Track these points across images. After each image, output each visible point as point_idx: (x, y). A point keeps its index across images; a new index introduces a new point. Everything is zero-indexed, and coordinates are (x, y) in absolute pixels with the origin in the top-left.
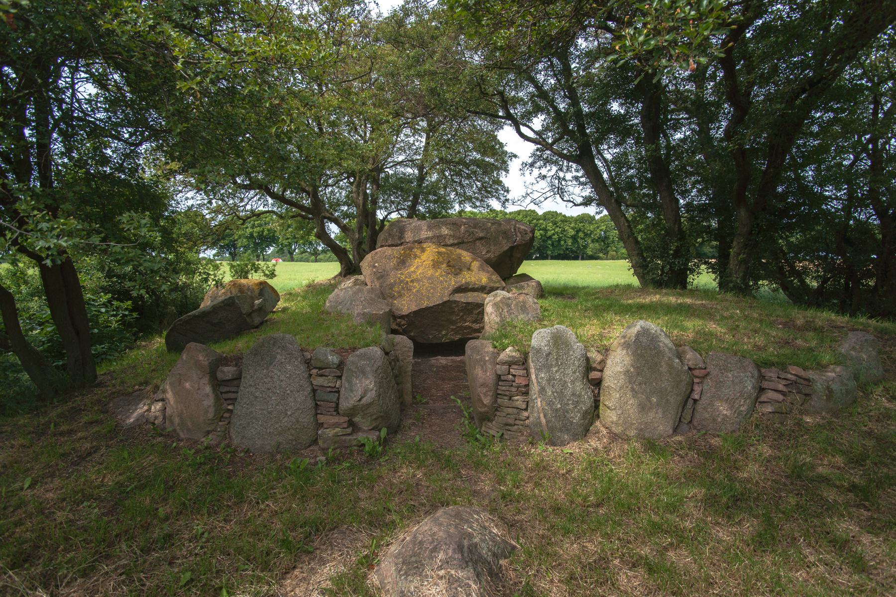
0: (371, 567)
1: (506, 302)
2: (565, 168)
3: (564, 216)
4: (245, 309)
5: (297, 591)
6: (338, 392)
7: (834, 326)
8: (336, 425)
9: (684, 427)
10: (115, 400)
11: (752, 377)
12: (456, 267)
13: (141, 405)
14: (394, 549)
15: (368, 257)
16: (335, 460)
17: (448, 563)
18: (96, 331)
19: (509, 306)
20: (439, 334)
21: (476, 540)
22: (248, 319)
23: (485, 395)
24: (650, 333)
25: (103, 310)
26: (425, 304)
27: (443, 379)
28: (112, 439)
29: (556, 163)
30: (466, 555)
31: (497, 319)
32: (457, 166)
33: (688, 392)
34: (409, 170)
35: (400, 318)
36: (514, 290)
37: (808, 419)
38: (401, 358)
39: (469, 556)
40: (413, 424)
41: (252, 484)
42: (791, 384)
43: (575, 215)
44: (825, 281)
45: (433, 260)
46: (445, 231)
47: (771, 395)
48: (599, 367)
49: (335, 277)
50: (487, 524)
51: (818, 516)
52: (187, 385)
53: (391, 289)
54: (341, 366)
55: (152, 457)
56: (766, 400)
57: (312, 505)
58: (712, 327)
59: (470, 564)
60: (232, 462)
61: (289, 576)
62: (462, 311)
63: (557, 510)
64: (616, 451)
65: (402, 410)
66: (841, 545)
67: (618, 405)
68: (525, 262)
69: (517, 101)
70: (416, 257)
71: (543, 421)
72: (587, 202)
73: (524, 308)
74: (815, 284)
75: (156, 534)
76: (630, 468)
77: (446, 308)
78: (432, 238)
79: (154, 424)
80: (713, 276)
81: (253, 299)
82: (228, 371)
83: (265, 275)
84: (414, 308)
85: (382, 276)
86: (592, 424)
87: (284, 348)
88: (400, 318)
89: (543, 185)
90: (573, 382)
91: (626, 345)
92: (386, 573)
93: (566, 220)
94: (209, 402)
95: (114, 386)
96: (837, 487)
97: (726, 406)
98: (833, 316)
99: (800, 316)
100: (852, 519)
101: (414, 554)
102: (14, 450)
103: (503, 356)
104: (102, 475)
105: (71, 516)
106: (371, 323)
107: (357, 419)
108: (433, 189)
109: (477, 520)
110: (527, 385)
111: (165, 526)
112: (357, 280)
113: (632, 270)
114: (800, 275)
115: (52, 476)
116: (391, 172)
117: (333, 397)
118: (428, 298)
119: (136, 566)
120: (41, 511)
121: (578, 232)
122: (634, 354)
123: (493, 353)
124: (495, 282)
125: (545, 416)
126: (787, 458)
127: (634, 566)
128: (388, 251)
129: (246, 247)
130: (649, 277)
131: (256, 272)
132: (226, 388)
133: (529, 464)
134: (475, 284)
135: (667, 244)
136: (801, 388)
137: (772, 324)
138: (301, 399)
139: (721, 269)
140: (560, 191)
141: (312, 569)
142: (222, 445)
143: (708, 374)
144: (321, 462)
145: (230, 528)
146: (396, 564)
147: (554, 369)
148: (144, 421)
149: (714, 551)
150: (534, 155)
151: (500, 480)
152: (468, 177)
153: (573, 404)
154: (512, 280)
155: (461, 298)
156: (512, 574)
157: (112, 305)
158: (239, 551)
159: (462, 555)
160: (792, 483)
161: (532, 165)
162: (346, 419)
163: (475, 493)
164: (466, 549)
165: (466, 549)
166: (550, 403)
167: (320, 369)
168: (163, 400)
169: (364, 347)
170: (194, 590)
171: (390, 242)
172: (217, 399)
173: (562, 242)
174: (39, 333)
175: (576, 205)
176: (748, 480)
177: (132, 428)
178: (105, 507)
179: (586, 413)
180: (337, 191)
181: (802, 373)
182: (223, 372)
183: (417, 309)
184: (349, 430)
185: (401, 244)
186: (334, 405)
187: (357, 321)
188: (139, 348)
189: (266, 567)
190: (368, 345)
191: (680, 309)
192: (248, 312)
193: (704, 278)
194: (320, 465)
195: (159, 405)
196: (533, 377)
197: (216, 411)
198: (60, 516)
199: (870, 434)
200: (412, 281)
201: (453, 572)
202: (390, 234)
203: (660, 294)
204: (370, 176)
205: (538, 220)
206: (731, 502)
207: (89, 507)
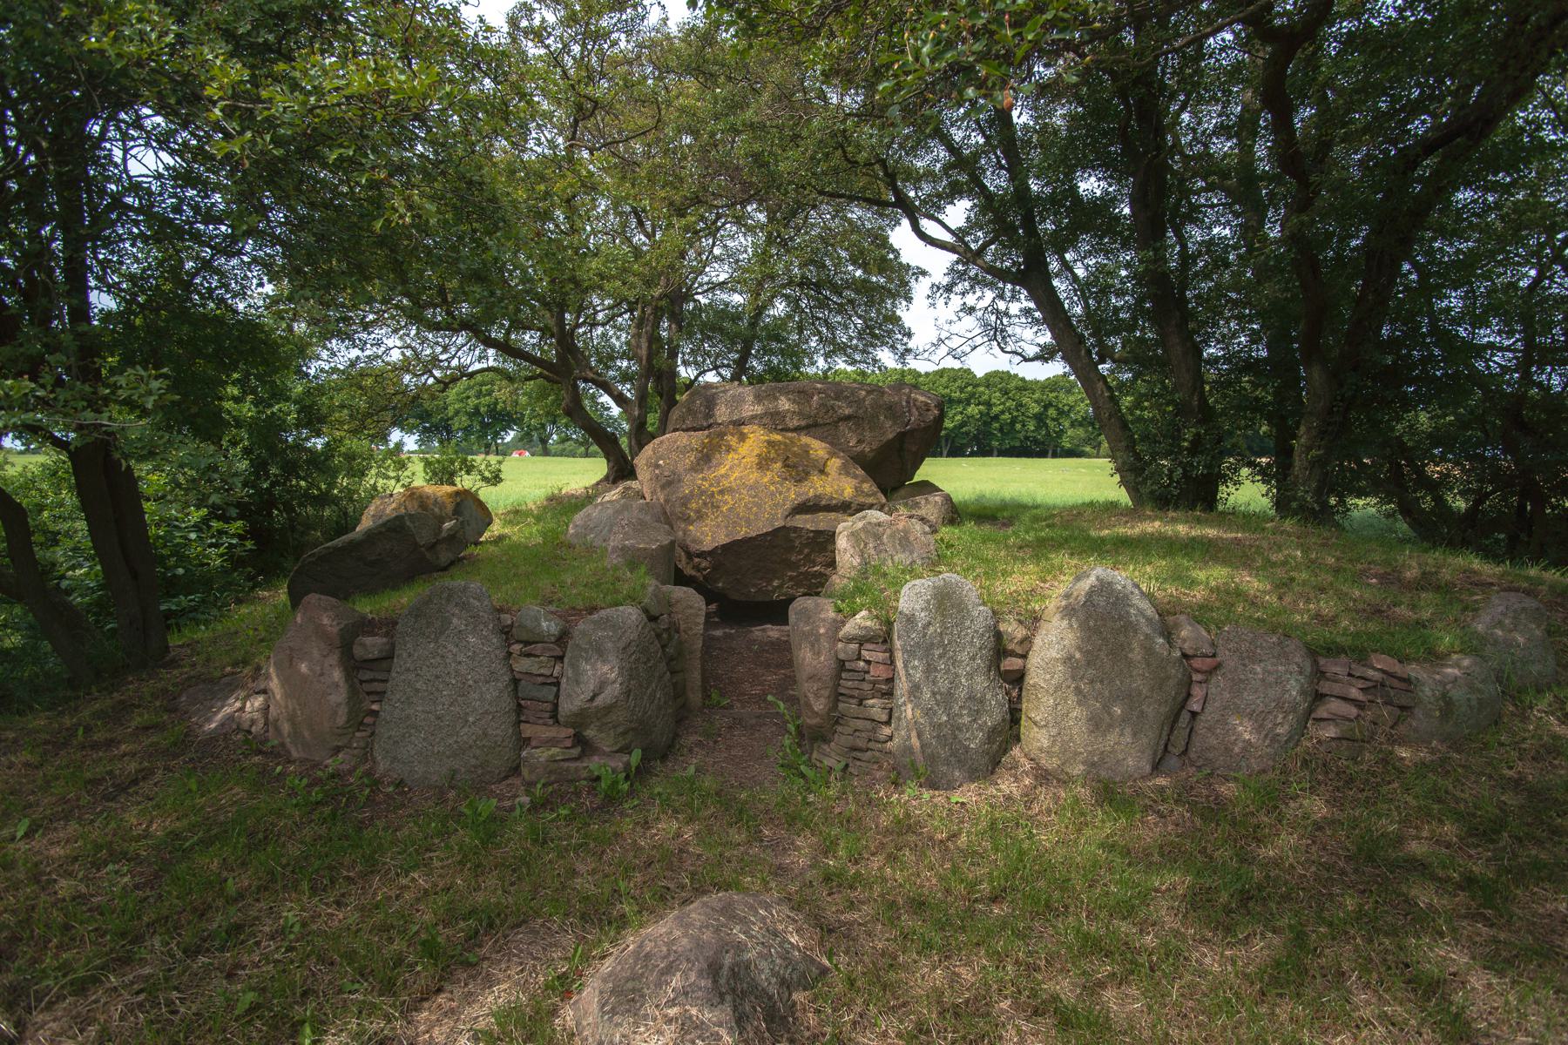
0: (567, 995)
1: (874, 531)
2: (1008, 294)
3: (1023, 379)
4: (424, 537)
5: (436, 1031)
6: (557, 684)
7: (1477, 583)
8: (552, 742)
9: (1173, 762)
10: (191, 690)
11: (1301, 673)
12: (798, 468)
13: (231, 700)
14: (607, 966)
15: (648, 450)
16: (544, 804)
17: (686, 994)
18: (181, 571)
19: (878, 537)
20: (756, 583)
21: (751, 955)
22: (428, 555)
23: (817, 696)
24: (1113, 590)
25: (193, 536)
26: (743, 532)
27: (768, 666)
28: (176, 756)
29: (991, 285)
30: (722, 981)
31: (856, 561)
32: (819, 288)
33: (1180, 699)
34: (737, 299)
35: (698, 556)
36: (903, 510)
37: (1404, 753)
38: (682, 627)
39: (730, 983)
40: (699, 744)
41: (394, 843)
42: (1373, 688)
43: (1042, 377)
44: (1481, 497)
45: (759, 455)
46: (784, 404)
47: (1335, 706)
48: (1019, 651)
49: (598, 484)
50: (780, 927)
51: (1393, 933)
52: (304, 668)
53: (685, 505)
54: (563, 638)
55: (237, 789)
56: (1325, 715)
57: (491, 881)
58: (1252, 583)
59: (728, 998)
60: (370, 801)
61: (426, 1005)
62: (806, 545)
63: (918, 905)
64: (1045, 798)
65: (679, 722)
66: (1429, 989)
67: (1053, 719)
68: (928, 460)
69: (916, 178)
70: (729, 449)
71: (915, 742)
72: (1045, 355)
73: (905, 542)
74: (1461, 504)
75: (217, 922)
76: (1064, 832)
77: (780, 539)
78: (761, 417)
79: (249, 732)
80: (1264, 488)
81: (442, 520)
82: (371, 645)
83: (484, 479)
84: (723, 539)
85: (669, 483)
86: (1005, 752)
87: (464, 606)
88: (698, 556)
89: (970, 322)
90: (970, 676)
91: (1069, 612)
92: (584, 1010)
93: (1025, 386)
94: (339, 697)
95: (194, 665)
96: (1440, 880)
97: (1248, 725)
98: (1476, 564)
99: (1412, 564)
100: (1457, 941)
101: (634, 977)
102: (12, 771)
103: (849, 628)
104: (146, 821)
105: (83, 889)
106: (633, 565)
107: (590, 733)
108: (776, 333)
109: (764, 918)
110: (890, 680)
111: (232, 910)
112: (627, 489)
113: (1117, 478)
114: (1436, 488)
115: (67, 818)
116: (703, 300)
117: (548, 692)
118: (748, 521)
119: (167, 979)
120: (35, 878)
121: (1046, 407)
122: (1084, 626)
123: (835, 621)
124: (868, 495)
125: (919, 736)
126: (1355, 823)
127: (1036, 1012)
128: (682, 439)
129: (467, 430)
130: (1145, 490)
131: (468, 473)
132: (367, 673)
133: (884, 821)
134: (832, 498)
135: (1179, 430)
136: (1395, 695)
137: (1359, 578)
138: (492, 695)
139: (1279, 477)
140: (997, 333)
141: (471, 994)
142: (359, 772)
143: (1218, 667)
144: (521, 806)
145: (348, 916)
146: (601, 993)
147: (937, 653)
148: (233, 726)
149: (1190, 991)
150: (952, 270)
151: (829, 849)
152: (841, 310)
153: (969, 715)
154: (902, 492)
155: (805, 522)
156: (812, 1019)
157: (209, 527)
158: (350, 956)
159: (715, 982)
160: (1356, 871)
161: (949, 289)
162: (571, 731)
163: (780, 871)
164: (725, 971)
165: (725, 971)
166: (928, 712)
167: (527, 643)
168: (264, 692)
169: (610, 606)
170: (258, 1024)
171: (689, 423)
172: (353, 692)
173: (1018, 426)
174: (87, 574)
175: (1026, 360)
176: (1277, 863)
177: (213, 739)
178: (142, 874)
179: (992, 733)
180: (609, 332)
181: (1397, 668)
182: (364, 645)
183: (728, 540)
184: (576, 752)
185: (709, 426)
186: (548, 707)
187: (615, 560)
188: (253, 601)
189: (388, 987)
190: (617, 604)
191: (1189, 547)
192: (435, 543)
193: (1248, 493)
194: (518, 811)
195: (258, 701)
196: (899, 664)
197: (350, 713)
198: (65, 887)
199: (1517, 784)
200: (721, 492)
201: (694, 1011)
202: (689, 410)
203: (1161, 519)
204: (666, 304)
205: (976, 386)
206: (1231, 904)
207: (116, 872)
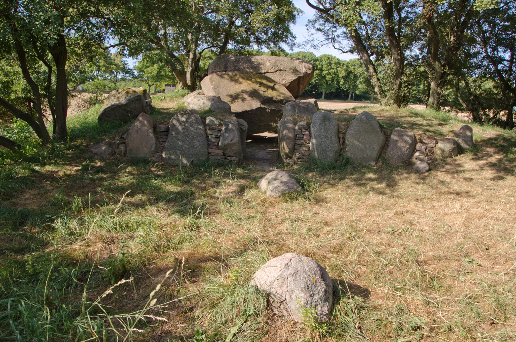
93: (338, 63)
175: (344, 52)
